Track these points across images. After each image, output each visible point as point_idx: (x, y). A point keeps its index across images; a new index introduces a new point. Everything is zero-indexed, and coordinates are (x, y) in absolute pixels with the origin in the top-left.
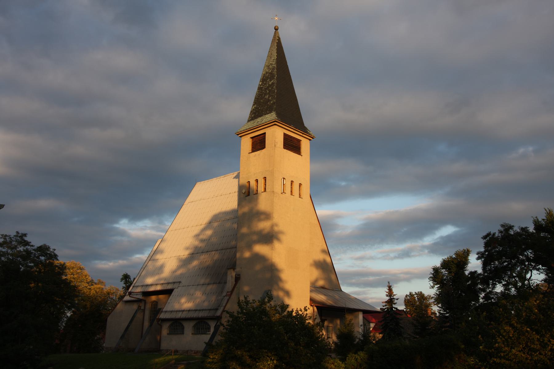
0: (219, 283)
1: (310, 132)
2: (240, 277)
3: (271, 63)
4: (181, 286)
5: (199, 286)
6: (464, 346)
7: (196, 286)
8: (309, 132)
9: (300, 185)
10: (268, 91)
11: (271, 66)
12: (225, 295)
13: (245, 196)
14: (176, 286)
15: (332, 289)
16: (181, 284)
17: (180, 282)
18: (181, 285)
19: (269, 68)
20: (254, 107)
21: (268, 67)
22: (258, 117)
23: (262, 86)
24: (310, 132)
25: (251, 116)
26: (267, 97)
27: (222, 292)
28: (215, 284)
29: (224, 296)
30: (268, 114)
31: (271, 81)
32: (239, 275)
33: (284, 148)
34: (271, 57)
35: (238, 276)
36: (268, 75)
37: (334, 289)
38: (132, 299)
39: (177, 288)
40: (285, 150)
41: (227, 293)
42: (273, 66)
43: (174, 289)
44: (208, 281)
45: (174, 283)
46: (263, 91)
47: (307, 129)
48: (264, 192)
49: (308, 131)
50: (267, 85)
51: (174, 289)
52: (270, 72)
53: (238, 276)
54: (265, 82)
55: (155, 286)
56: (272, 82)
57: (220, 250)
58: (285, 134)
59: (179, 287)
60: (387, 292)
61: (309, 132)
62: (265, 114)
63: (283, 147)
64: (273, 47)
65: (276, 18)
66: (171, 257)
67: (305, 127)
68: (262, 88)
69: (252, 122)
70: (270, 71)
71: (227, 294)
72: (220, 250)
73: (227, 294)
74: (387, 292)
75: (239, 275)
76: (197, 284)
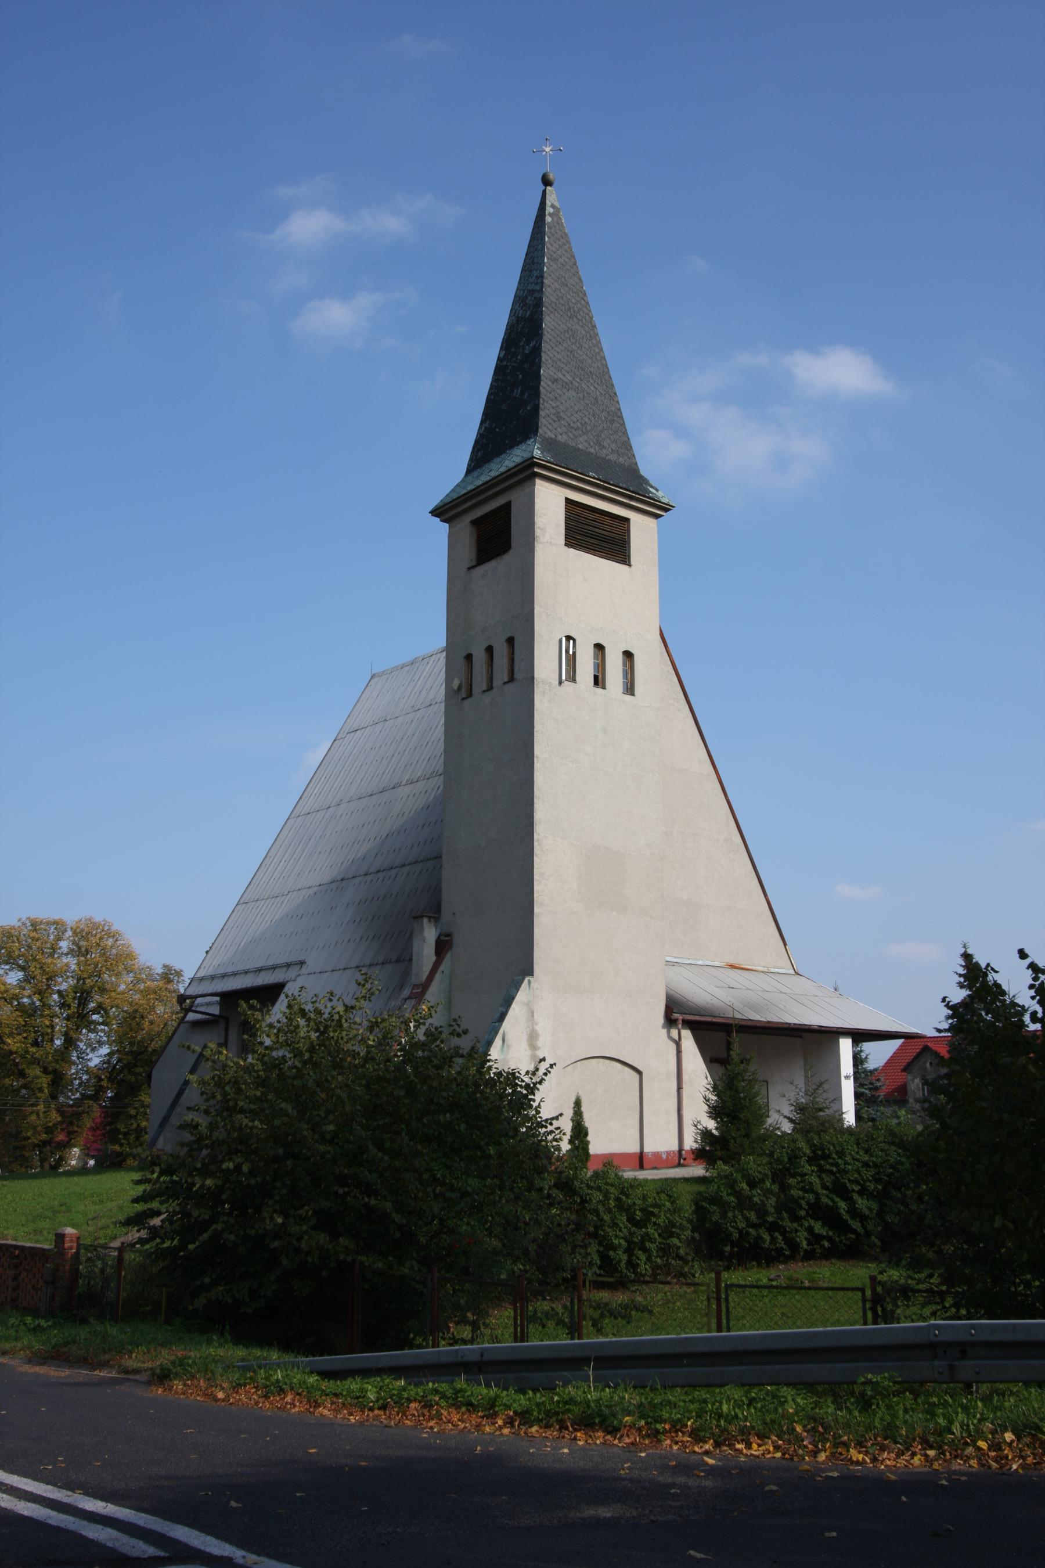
0: (398, 961)
1: (657, 490)
2: (452, 939)
3: (530, 287)
4: (303, 975)
5: (346, 971)
6: (502, 1277)
7: (341, 972)
8: (654, 491)
9: (628, 655)
10: (520, 376)
11: (529, 298)
12: (407, 997)
13: (460, 698)
14: (292, 973)
15: (765, 970)
16: (304, 967)
17: (302, 963)
18: (305, 970)
19: (525, 304)
20: (483, 428)
21: (522, 301)
22: (493, 458)
23: (505, 363)
24: (657, 490)
25: (476, 456)
26: (517, 393)
27: (401, 987)
28: (386, 963)
29: (406, 999)
30: (520, 443)
31: (528, 344)
32: (449, 935)
33: (566, 545)
34: (531, 271)
35: (447, 938)
36: (523, 325)
37: (772, 970)
38: (195, 1018)
39: (295, 980)
40: (572, 550)
41: (413, 989)
42: (535, 298)
43: (288, 982)
44: (963, 972)
45: (288, 965)
46: (509, 378)
47: (647, 482)
48: (509, 684)
49: (651, 489)
50: (519, 357)
51: (288, 982)
52: (527, 316)
53: (447, 938)
54: (513, 350)
55: (242, 976)
56: (531, 345)
57: (409, 864)
58: (568, 501)
59: (299, 975)
60: (960, 975)
61: (654, 491)
62: (512, 447)
63: (563, 542)
64: (538, 240)
65: (548, 149)
66: (289, 892)
67: (642, 477)
68: (506, 367)
69: (476, 473)
70: (528, 313)
71: (414, 991)
72: (409, 864)
73: (414, 991)
74: (960, 975)
75: (449, 935)
76: (342, 967)
